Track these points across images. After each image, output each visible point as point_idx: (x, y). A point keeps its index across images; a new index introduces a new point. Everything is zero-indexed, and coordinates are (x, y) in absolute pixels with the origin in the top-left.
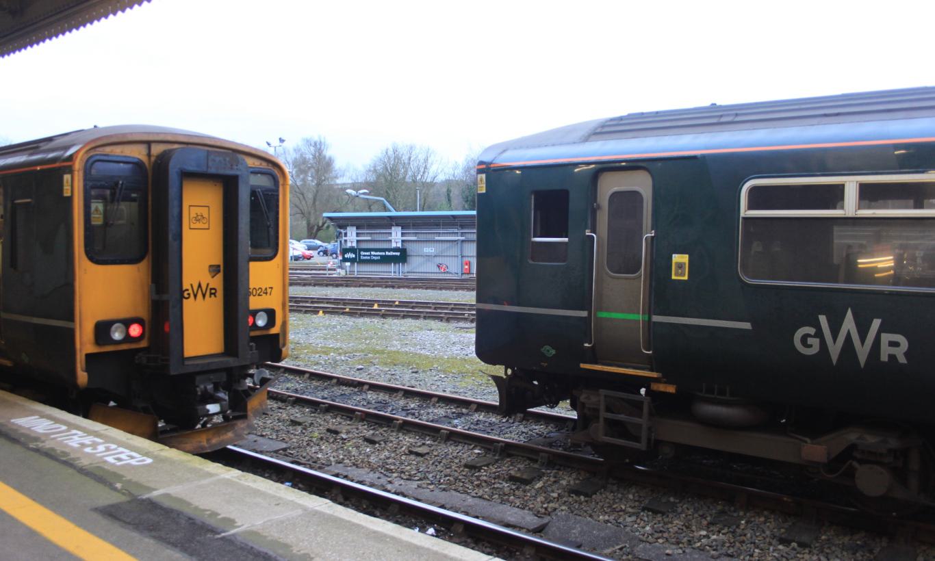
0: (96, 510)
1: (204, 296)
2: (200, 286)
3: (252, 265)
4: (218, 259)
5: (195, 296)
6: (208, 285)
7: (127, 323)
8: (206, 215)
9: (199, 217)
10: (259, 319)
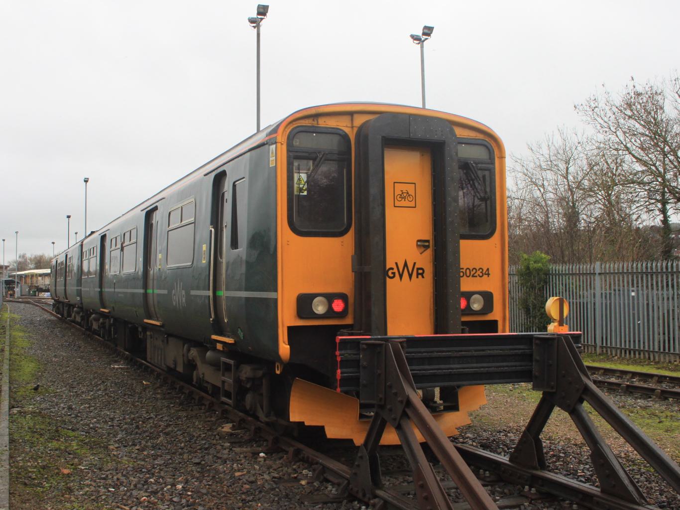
0: (406, 261)
1: (410, 276)
2: (406, 265)
3: (464, 243)
4: (426, 233)
5: (401, 276)
6: (415, 263)
7: (330, 298)
8: (412, 192)
9: (405, 195)
10: (474, 303)
